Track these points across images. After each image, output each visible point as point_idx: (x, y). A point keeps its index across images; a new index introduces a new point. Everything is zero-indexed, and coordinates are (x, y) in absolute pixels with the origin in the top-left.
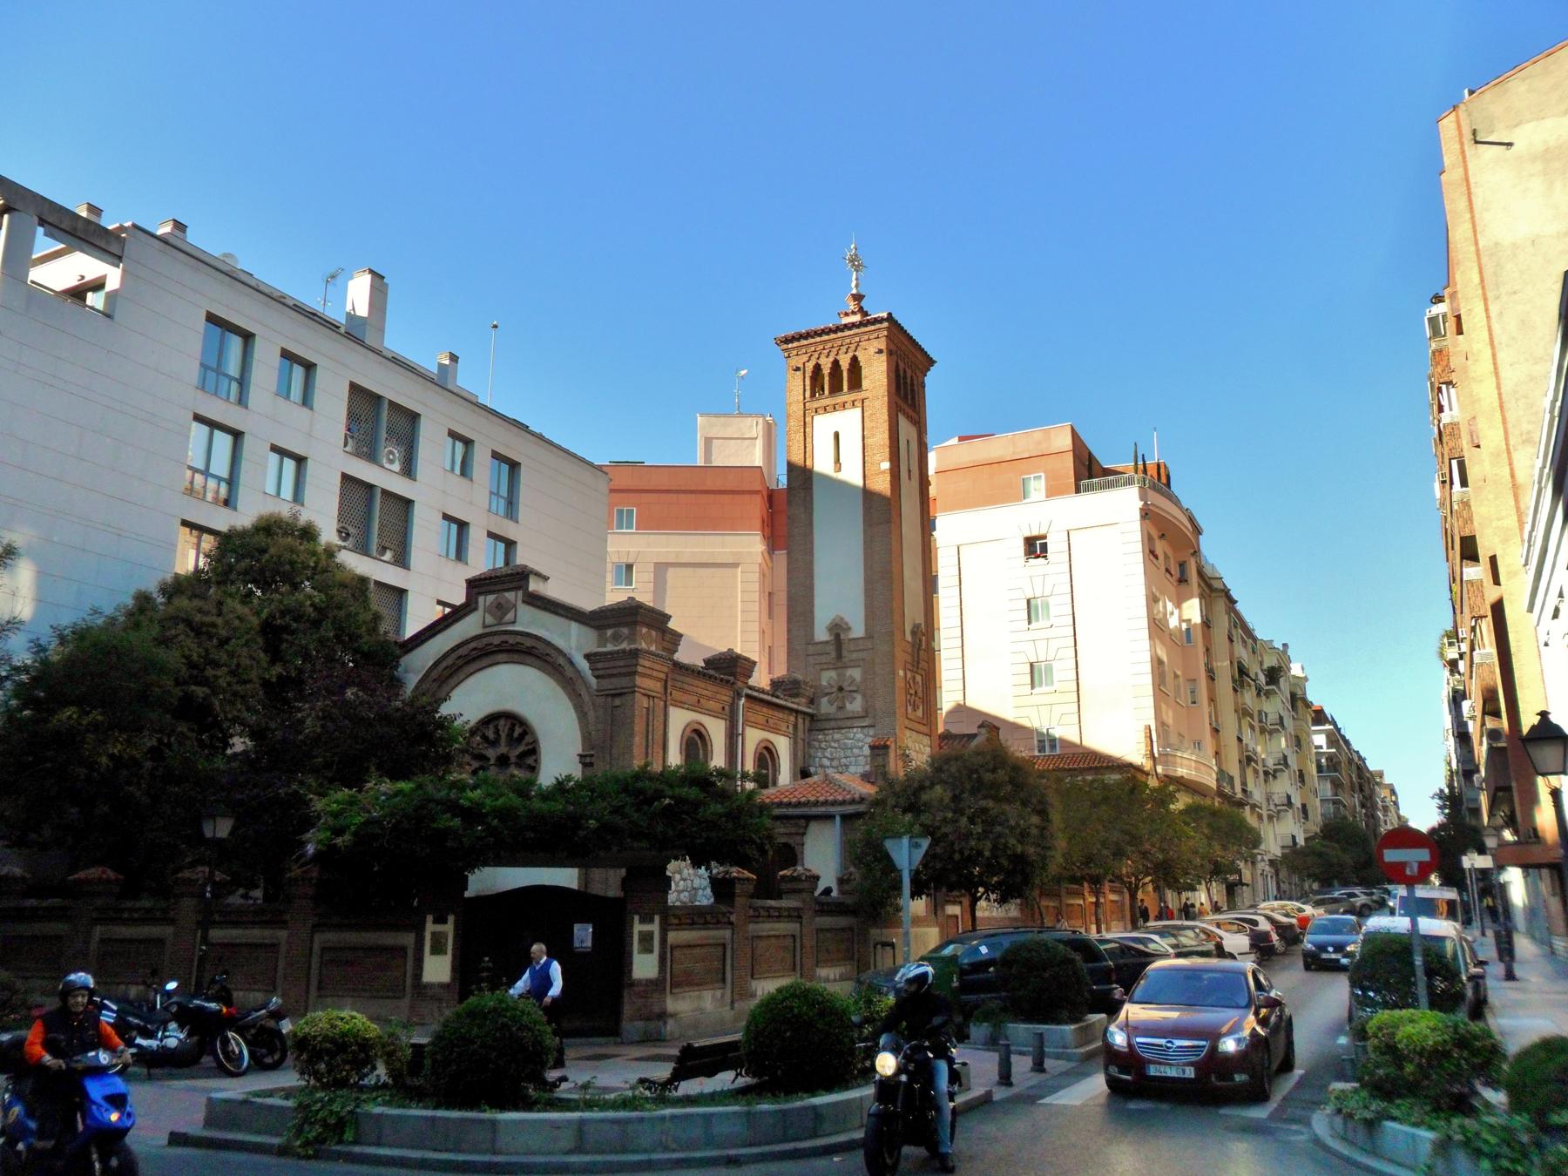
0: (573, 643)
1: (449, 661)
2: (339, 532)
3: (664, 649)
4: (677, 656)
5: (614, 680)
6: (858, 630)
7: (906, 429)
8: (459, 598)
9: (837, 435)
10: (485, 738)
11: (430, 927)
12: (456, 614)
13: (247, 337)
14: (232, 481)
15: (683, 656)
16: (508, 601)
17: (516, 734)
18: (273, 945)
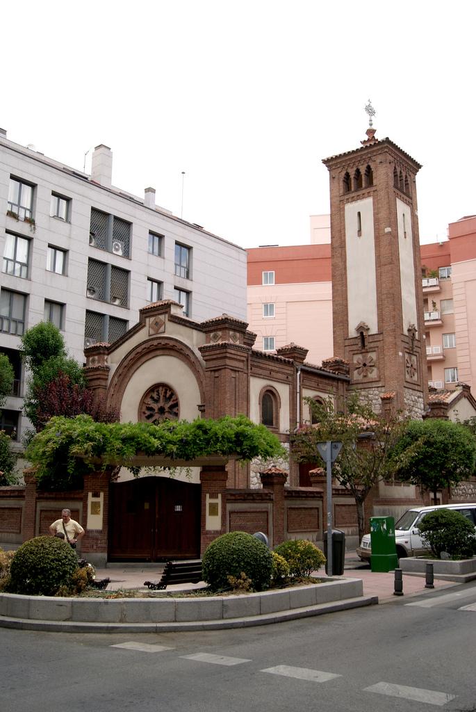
0: (195, 342)
1: (132, 356)
3: (245, 343)
5: (215, 362)
6: (374, 330)
7: (402, 208)
9: (359, 214)
10: (152, 398)
11: (91, 499)
13: (33, 186)
14: (27, 265)
15: (258, 346)
16: (161, 320)
17: (168, 396)
18: (18, 509)
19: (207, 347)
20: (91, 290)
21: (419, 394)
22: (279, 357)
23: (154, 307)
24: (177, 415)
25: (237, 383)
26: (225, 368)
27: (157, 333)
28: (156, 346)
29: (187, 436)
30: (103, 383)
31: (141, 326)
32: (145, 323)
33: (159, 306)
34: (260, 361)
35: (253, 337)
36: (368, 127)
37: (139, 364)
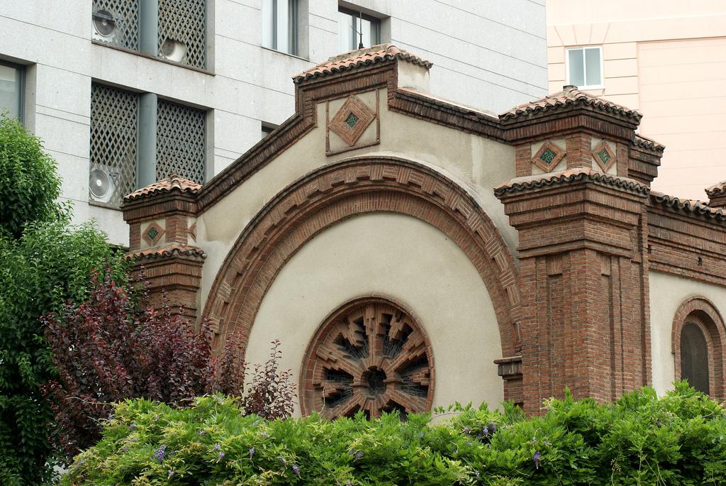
2: (96, 19)
3: (632, 173)
4: (659, 187)
5: (548, 230)
8: (282, 110)
10: (343, 342)
12: (277, 139)
16: (365, 109)
17: (393, 333)
19: (524, 187)
22: (713, 210)
23: (343, 69)
24: (424, 390)
25: (616, 291)
26: (584, 248)
27: (353, 148)
28: (351, 185)
29: (544, 451)
30: (186, 300)
31: (301, 127)
32: (314, 115)
33: (360, 65)
34: (675, 224)
37: (297, 240)
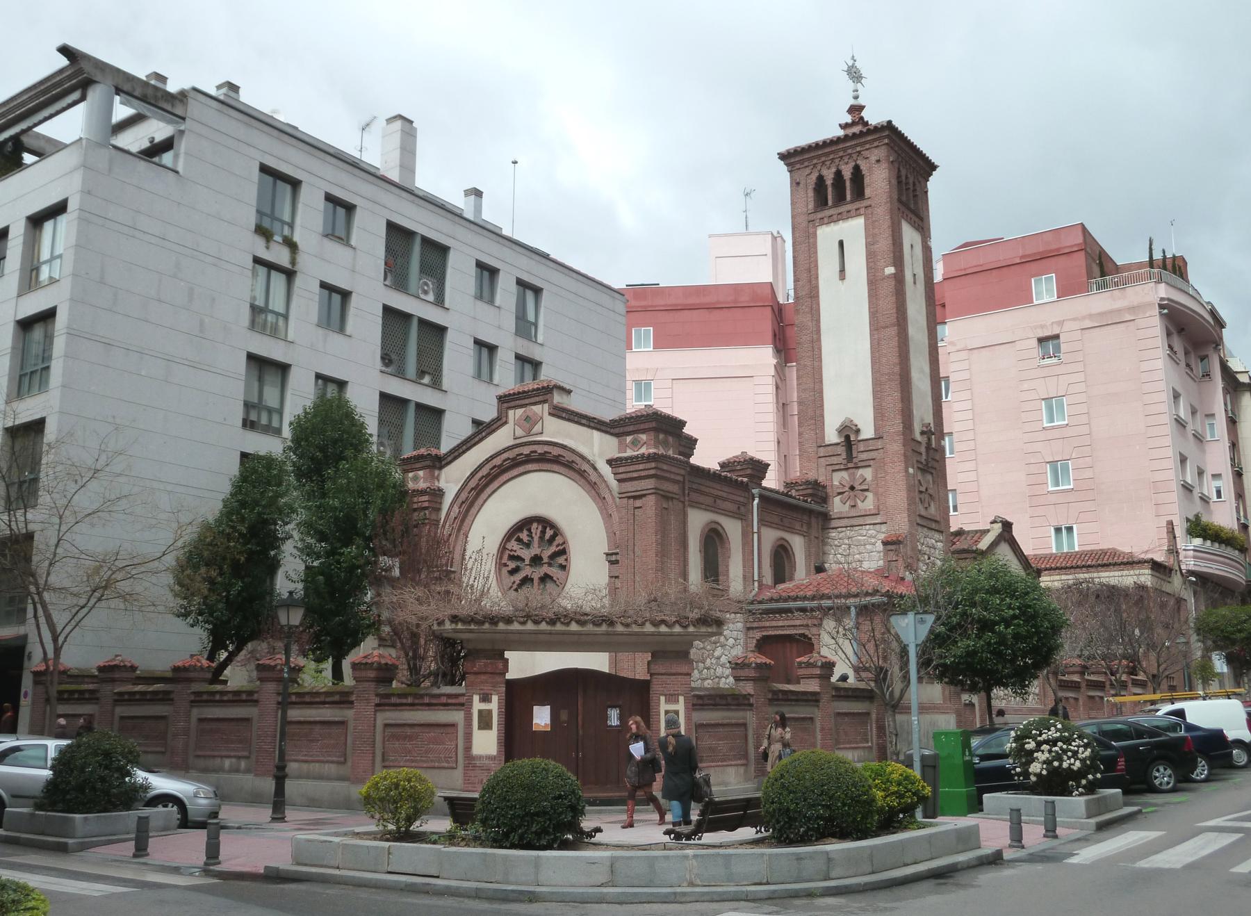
0: (596, 449)
1: (485, 471)
6: (868, 432)
7: (909, 235)
9: (841, 244)
11: (477, 705)
16: (535, 414)
17: (547, 536)
19: (620, 459)
20: (386, 359)
21: (937, 536)
23: (524, 392)
35: (691, 443)
36: (853, 102)
